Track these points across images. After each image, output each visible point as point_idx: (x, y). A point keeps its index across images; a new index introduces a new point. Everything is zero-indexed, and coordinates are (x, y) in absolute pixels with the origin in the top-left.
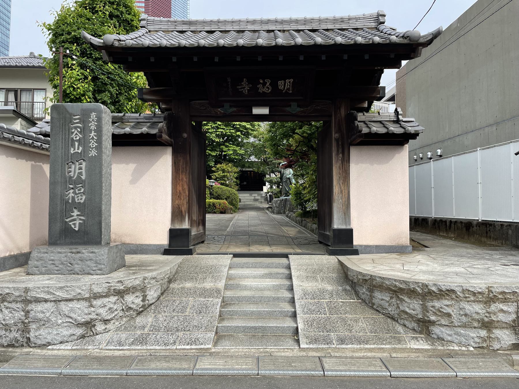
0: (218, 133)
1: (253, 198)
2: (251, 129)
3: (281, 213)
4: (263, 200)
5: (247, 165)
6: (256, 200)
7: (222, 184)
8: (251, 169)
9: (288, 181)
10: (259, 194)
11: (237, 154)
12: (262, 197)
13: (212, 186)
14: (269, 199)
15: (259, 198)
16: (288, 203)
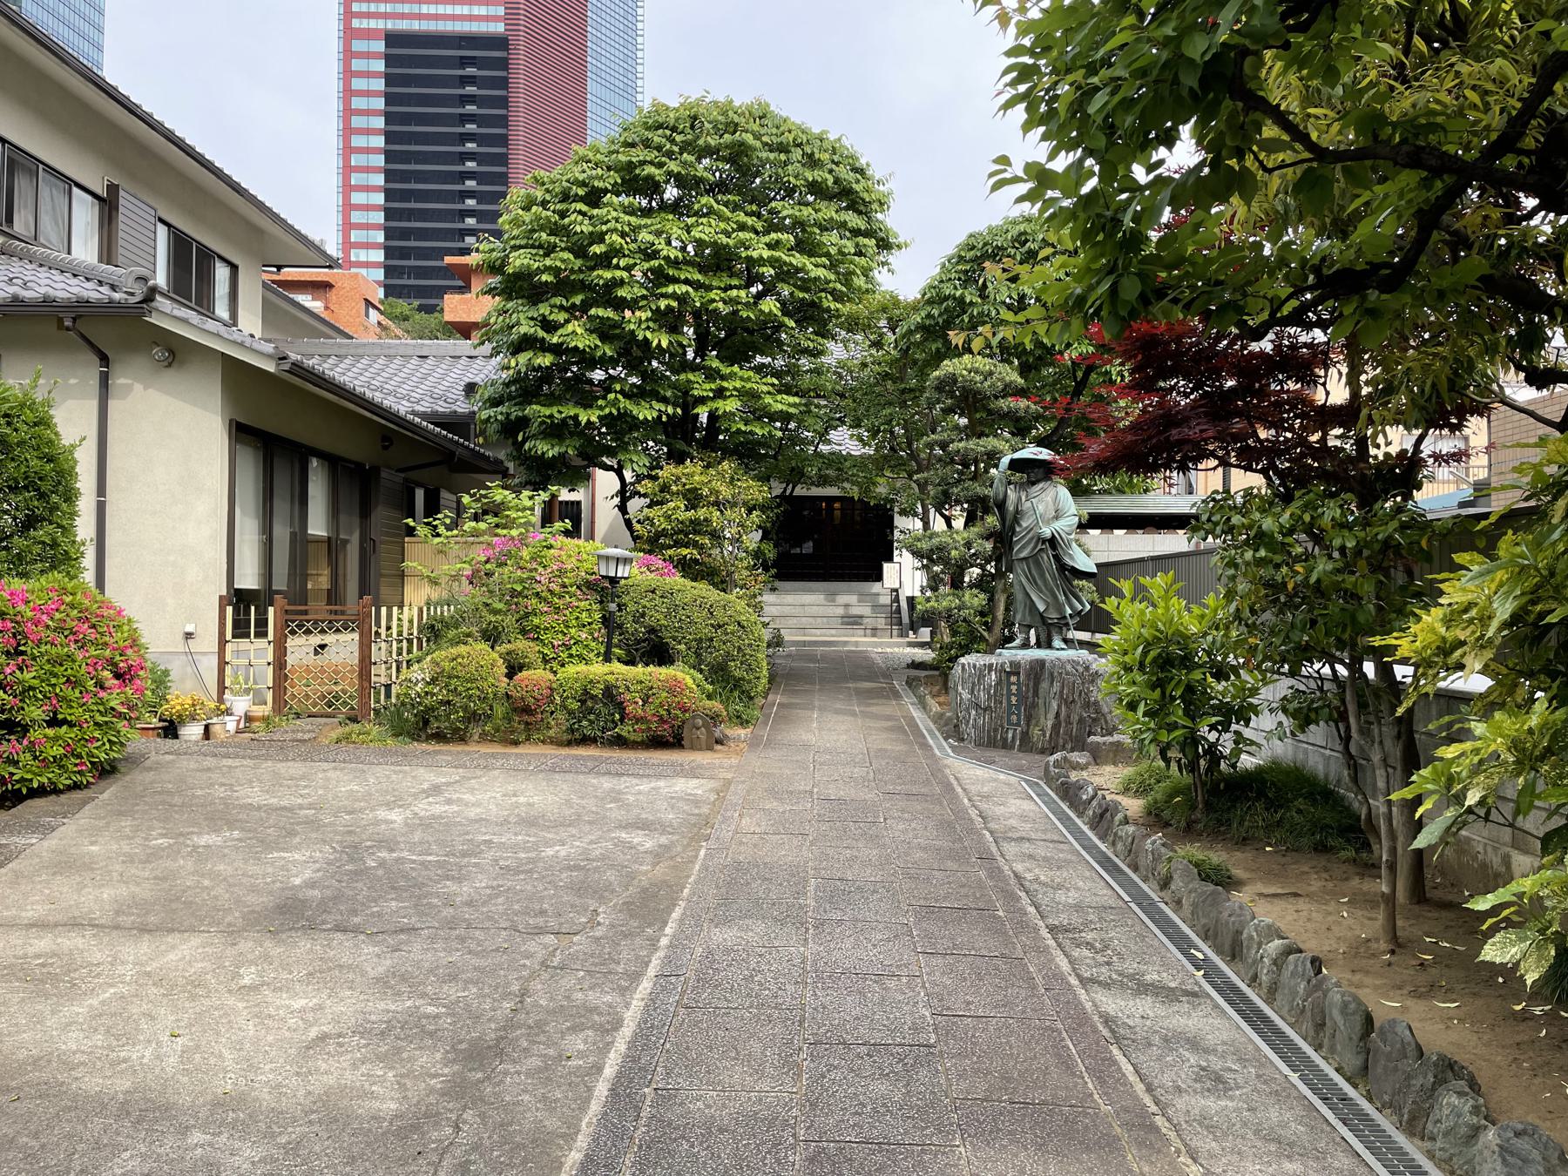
0: (663, 304)
1: (840, 611)
2: (833, 292)
3: (1006, 745)
4: (881, 623)
5: (812, 471)
6: (852, 621)
7: (688, 568)
8: (832, 491)
9: (1047, 559)
10: (863, 596)
11: (761, 414)
12: (876, 607)
13: (614, 581)
14: (906, 619)
15: (865, 610)
16: (1050, 691)
